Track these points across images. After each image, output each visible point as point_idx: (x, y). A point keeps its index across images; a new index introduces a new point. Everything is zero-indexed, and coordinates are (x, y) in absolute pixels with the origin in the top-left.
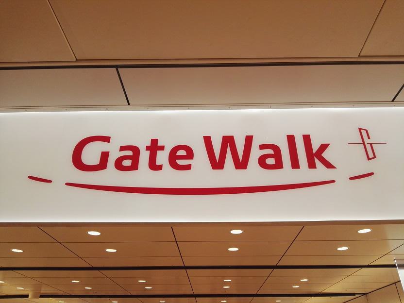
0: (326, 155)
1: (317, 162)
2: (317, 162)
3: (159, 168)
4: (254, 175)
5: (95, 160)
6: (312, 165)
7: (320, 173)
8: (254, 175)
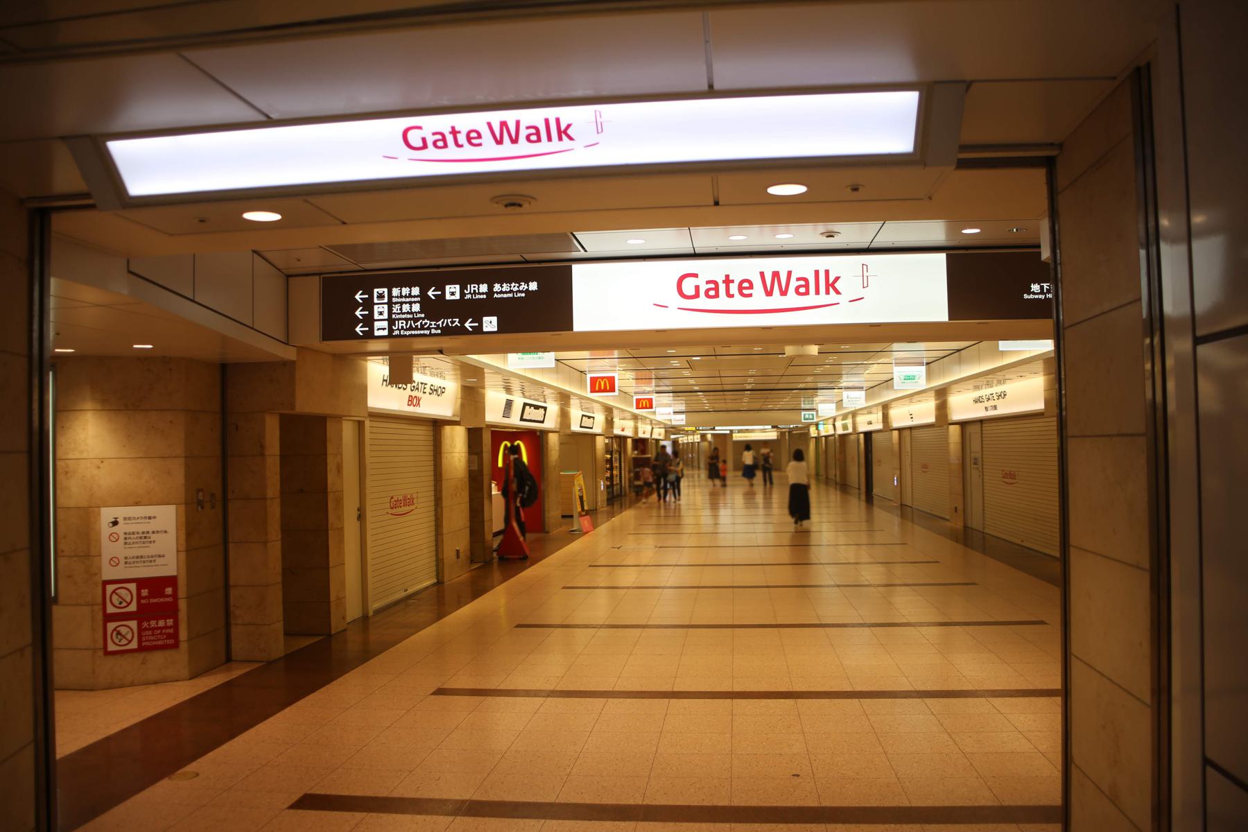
0: (569, 132)
1: (564, 136)
2: (564, 136)
3: (732, 296)
4: (792, 300)
5: (690, 292)
6: (560, 139)
7: (833, 297)
8: (792, 300)
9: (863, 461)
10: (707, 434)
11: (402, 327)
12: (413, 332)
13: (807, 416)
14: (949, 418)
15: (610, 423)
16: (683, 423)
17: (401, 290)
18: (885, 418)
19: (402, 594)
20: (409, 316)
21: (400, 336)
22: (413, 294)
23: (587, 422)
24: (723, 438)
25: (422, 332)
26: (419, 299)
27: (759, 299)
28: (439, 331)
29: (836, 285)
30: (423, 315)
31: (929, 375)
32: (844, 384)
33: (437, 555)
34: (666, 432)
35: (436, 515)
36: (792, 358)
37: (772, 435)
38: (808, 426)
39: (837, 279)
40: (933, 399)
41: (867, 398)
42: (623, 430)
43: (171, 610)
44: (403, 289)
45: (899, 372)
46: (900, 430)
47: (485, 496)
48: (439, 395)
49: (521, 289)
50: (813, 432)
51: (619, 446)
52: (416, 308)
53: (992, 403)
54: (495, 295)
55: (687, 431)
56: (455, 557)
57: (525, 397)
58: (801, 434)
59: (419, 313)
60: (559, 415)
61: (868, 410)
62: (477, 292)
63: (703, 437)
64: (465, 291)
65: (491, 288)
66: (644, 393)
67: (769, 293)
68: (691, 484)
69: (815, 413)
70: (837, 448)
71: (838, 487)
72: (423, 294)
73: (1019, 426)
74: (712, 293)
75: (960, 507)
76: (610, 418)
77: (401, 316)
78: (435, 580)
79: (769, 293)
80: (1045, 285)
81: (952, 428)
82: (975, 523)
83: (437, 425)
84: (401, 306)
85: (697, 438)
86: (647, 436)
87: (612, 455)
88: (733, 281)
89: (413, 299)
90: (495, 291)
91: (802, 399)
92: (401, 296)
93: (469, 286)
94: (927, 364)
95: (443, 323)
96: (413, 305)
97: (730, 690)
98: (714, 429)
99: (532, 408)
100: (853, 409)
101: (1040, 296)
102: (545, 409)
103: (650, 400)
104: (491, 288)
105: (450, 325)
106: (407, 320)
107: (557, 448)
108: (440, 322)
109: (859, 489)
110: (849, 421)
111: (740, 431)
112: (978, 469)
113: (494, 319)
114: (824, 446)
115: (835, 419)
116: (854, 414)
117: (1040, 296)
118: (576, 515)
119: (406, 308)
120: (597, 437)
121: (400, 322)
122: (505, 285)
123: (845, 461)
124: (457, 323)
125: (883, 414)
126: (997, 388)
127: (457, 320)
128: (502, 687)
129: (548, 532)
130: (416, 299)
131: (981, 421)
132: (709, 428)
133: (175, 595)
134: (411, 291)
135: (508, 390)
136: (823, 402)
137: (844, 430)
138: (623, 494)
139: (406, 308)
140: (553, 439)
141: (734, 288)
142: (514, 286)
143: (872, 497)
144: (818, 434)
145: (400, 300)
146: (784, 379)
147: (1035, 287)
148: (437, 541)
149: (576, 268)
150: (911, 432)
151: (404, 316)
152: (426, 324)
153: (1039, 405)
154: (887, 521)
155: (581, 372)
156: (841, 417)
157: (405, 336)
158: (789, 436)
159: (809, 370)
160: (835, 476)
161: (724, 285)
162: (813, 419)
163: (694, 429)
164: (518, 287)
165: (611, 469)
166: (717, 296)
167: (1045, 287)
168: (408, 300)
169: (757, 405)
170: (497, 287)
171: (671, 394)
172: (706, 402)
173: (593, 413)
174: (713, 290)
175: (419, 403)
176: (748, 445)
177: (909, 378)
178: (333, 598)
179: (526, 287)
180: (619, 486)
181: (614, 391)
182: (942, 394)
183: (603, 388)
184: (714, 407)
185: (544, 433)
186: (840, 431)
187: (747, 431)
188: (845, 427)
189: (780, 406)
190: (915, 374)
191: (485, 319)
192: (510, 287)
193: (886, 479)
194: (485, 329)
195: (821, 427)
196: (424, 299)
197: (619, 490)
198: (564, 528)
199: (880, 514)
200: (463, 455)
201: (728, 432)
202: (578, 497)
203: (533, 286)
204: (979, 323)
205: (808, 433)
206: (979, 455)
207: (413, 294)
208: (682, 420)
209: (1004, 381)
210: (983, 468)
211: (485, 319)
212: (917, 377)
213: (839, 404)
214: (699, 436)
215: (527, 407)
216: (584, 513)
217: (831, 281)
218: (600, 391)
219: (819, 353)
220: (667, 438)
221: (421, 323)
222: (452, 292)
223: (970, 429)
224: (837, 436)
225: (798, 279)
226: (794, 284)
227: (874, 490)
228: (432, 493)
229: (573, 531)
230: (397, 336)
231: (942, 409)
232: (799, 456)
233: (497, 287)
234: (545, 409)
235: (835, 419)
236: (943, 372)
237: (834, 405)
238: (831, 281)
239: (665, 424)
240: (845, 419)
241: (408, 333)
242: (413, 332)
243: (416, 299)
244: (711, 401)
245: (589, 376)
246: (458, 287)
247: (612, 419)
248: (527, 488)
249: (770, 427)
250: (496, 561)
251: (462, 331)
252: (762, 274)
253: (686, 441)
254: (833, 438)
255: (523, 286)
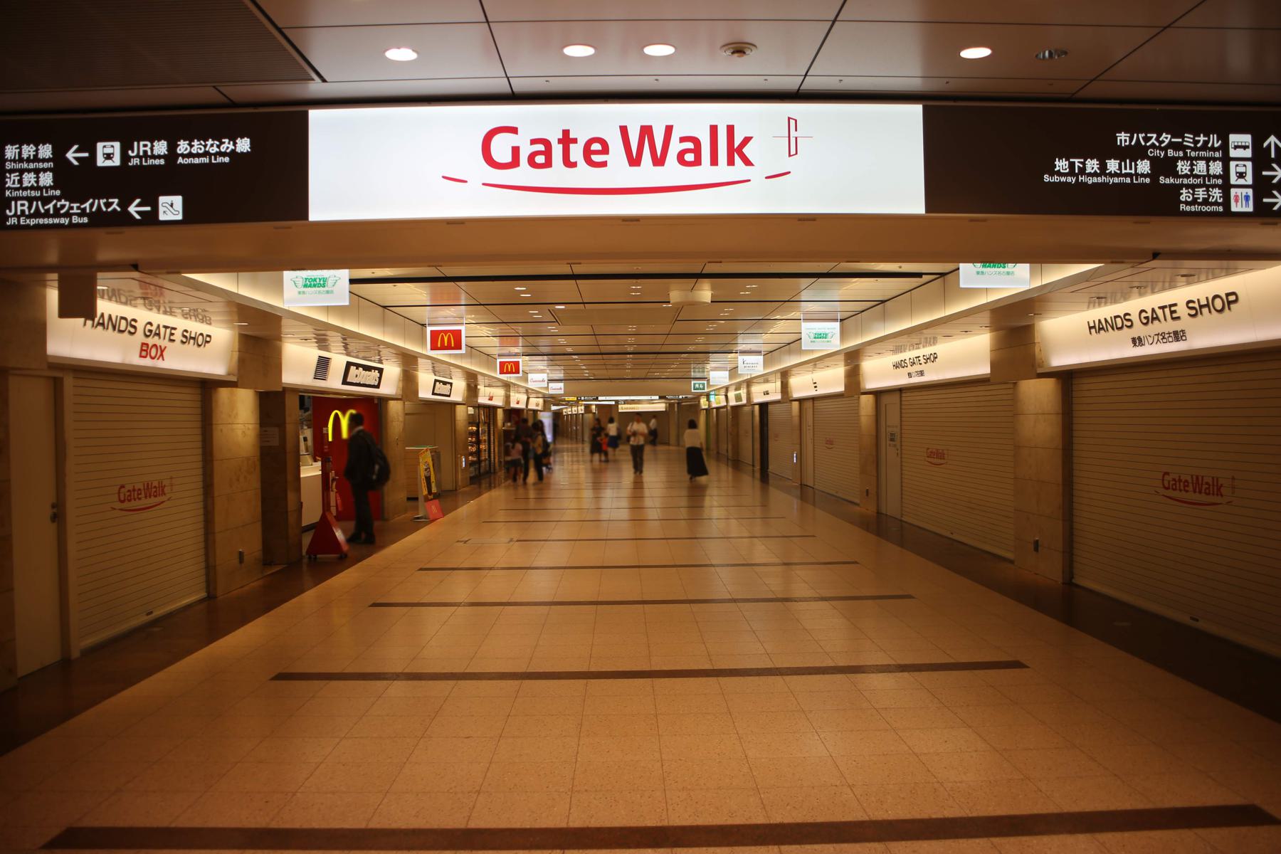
3: (574, 165)
4: (672, 173)
9: (757, 435)
10: (591, 405)
11: (23, 211)
12: (41, 221)
13: (697, 386)
14: (862, 386)
15: (472, 390)
16: (562, 392)
17: (20, 148)
18: (785, 388)
19: (144, 619)
20: (33, 194)
21: (17, 227)
22: (40, 156)
23: (441, 388)
24: (608, 412)
25: (56, 221)
26: (51, 165)
27: (617, 171)
28: (85, 220)
29: (745, 150)
30: (58, 193)
31: (844, 334)
32: (740, 347)
33: (207, 561)
34: (544, 401)
35: (205, 508)
36: (680, 307)
37: (660, 407)
38: (698, 397)
39: (747, 140)
40: (842, 363)
41: (766, 363)
42: (491, 399)
44: (25, 147)
45: (808, 329)
46: (801, 400)
47: (290, 478)
48: (199, 346)
49: (223, 150)
50: (703, 403)
51: (488, 417)
52: (47, 179)
53: (917, 368)
54: (180, 160)
55: (569, 401)
56: (237, 561)
57: (348, 354)
58: (691, 406)
59: (51, 188)
60: (401, 379)
61: (765, 378)
62: (149, 153)
63: (587, 408)
64: (130, 152)
65: (172, 147)
66: (510, 355)
67: (634, 161)
68: (575, 459)
69: (705, 382)
70: (730, 421)
71: (730, 463)
72: (59, 156)
73: (952, 396)
74: (540, 159)
76: (473, 385)
77: (20, 193)
78: (203, 594)
79: (634, 161)
80: (1076, 161)
81: (863, 398)
82: (891, 507)
83: (206, 387)
84: (21, 175)
85: (581, 409)
86: (522, 406)
87: (478, 427)
88: (575, 141)
89: (41, 165)
90: (179, 152)
91: (692, 366)
92: (21, 160)
93: (136, 143)
94: (841, 320)
95: (92, 205)
96: (41, 175)
97: (563, 825)
98: (596, 399)
99: (361, 369)
100: (749, 377)
101: (1069, 179)
102: (451, 384)
103: (517, 364)
104: (172, 147)
105: (104, 209)
106: (30, 200)
107: (401, 419)
108: (87, 205)
109: (753, 466)
110: (743, 392)
111: (626, 402)
112: (895, 446)
113: (178, 200)
114: (715, 419)
115: (727, 389)
116: (749, 383)
117: (1069, 179)
118: (421, 499)
119: (29, 179)
120: (458, 406)
121: (19, 203)
122: (196, 143)
123: (738, 435)
124: (115, 206)
125: (782, 382)
126: (911, 352)
127: (116, 201)
128: (186, 821)
129: (387, 520)
130: (46, 165)
131: (900, 390)
132: (591, 398)
134: (37, 151)
135: (322, 343)
136: (715, 369)
137: (737, 402)
138: (492, 471)
139: (29, 179)
140: (395, 408)
141: (576, 152)
142: (212, 145)
143: (768, 475)
144: (709, 405)
145: (18, 166)
146: (671, 339)
147: (1062, 165)
148: (206, 541)
149: (315, 115)
150: (901, 394)
151: (25, 194)
152: (63, 206)
153: (984, 369)
154: (784, 502)
155: (385, 307)
156: (734, 387)
157: (28, 227)
158: (678, 407)
159: (699, 326)
160: (727, 451)
161: (561, 146)
162: (704, 389)
163: (575, 399)
164: (218, 147)
165: (478, 442)
166: (548, 164)
167: (1077, 164)
168: (32, 166)
169: (642, 373)
170: (183, 146)
171: (545, 357)
172: (584, 367)
173: (451, 378)
174: (542, 156)
175: (162, 355)
176: (640, 416)
177: (819, 336)
179: (231, 147)
180: (487, 462)
181: (460, 349)
182: (853, 358)
183: (446, 344)
184: (594, 375)
185: (383, 400)
186: (733, 403)
187: (633, 402)
188: (738, 398)
189: (668, 374)
190: (827, 331)
191: (162, 199)
192: (205, 146)
193: (784, 455)
194: (162, 217)
195: (712, 398)
196: (59, 164)
197: (488, 466)
198: (409, 515)
199: (776, 494)
200: (251, 427)
201: (613, 403)
202: (423, 477)
203: (244, 145)
204: (972, 220)
205: (699, 404)
206: (897, 430)
207: (40, 156)
208: (561, 389)
209: (934, 341)
210: (901, 446)
211: (162, 199)
212: (829, 335)
213: (733, 371)
214: (583, 407)
215: (438, 383)
216: (431, 497)
217: (737, 143)
218: (443, 348)
219: (712, 302)
220: (546, 407)
221: (55, 206)
222: (108, 154)
223: (886, 399)
224: (729, 408)
225: (683, 140)
226: (675, 147)
227: (770, 467)
228: (200, 478)
229: (418, 518)
230: (13, 227)
231: (853, 375)
232: (693, 425)
233: (183, 146)
234: (451, 384)
235: (727, 389)
236: (861, 330)
237: (728, 372)
238: (737, 143)
239: (544, 394)
240: (740, 389)
241: (32, 222)
242: (41, 221)
243: (46, 165)
244: (590, 367)
245: (429, 329)
246: (117, 145)
247: (476, 386)
248: (377, 467)
249: (657, 397)
250: (305, 560)
251: (123, 219)
252: (624, 130)
253: (570, 413)
254: (725, 410)
255: (227, 146)
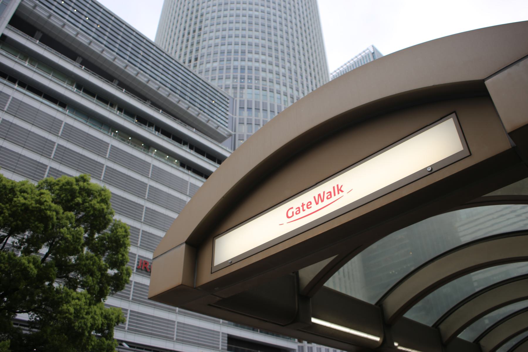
43: (244, 78)
67: (317, 203)
75: (232, 263)
88: (305, 205)
133: (248, 81)
178: (142, 124)
226: (326, 195)
